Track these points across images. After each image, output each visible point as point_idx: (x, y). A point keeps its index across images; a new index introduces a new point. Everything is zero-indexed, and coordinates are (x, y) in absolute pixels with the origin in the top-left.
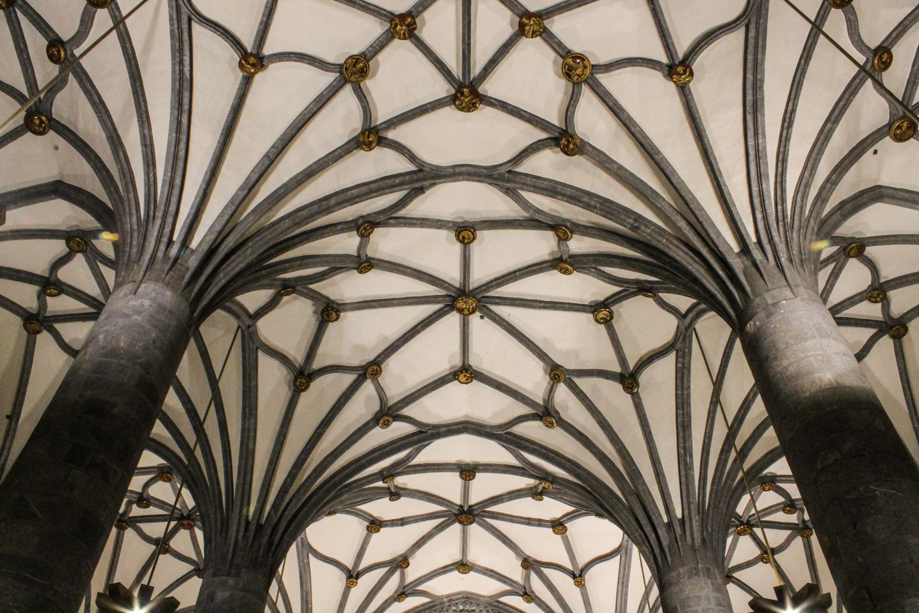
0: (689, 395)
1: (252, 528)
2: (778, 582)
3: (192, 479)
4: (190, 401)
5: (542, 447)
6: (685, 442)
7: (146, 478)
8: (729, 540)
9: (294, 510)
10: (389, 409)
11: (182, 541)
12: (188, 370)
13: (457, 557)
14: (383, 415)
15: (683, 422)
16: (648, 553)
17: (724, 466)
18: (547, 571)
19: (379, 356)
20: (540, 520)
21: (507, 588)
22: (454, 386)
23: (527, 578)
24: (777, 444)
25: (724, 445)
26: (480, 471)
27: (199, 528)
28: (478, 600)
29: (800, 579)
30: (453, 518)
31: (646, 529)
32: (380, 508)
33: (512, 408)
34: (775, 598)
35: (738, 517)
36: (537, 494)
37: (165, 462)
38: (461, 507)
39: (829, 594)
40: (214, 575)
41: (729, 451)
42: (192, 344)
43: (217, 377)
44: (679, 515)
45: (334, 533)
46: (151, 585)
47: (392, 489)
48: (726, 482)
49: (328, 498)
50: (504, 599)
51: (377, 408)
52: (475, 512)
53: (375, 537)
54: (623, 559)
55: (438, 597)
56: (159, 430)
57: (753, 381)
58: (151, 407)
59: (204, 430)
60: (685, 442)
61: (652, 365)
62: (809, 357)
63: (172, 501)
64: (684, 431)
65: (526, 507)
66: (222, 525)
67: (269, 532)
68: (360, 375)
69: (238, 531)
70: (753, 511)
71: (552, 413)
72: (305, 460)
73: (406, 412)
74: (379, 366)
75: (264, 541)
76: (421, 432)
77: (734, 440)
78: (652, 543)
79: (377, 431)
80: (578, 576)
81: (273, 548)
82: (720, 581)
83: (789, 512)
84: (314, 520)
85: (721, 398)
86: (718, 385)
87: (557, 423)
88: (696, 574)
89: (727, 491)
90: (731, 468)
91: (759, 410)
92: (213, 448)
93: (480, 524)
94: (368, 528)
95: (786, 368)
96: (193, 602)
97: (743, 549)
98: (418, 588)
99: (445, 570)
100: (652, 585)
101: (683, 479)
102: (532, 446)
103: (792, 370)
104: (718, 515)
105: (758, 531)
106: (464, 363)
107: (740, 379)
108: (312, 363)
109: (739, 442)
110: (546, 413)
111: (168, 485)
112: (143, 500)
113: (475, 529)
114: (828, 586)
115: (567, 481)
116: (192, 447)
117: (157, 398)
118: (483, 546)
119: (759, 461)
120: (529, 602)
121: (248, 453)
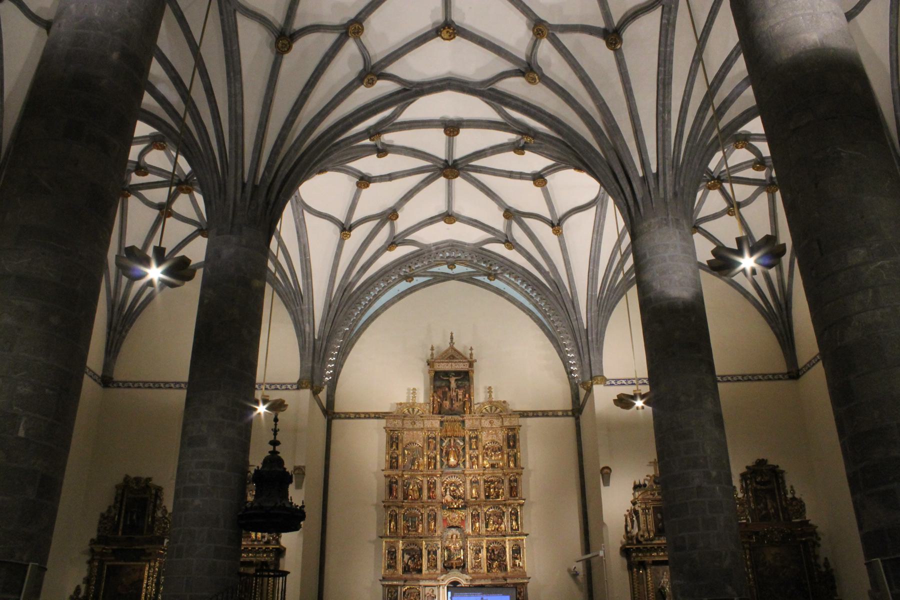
0: (671, 53)
1: (249, 189)
2: (740, 233)
3: (186, 147)
4: (173, 69)
5: (524, 102)
6: (664, 100)
7: (142, 147)
8: (699, 194)
9: (287, 171)
10: (373, 67)
11: (182, 204)
12: (168, 38)
13: (443, 209)
14: (368, 74)
15: (664, 79)
16: (622, 205)
17: (701, 124)
18: (528, 221)
19: (360, 14)
20: (521, 173)
21: (489, 236)
22: (437, 42)
23: (509, 227)
24: (754, 103)
25: (702, 103)
26: (463, 127)
27: (197, 191)
28: (463, 247)
29: (761, 230)
30: (439, 172)
31: (621, 183)
32: (369, 164)
33: (496, 65)
34: (735, 247)
35: (710, 173)
36: (518, 148)
37: (155, 131)
38: (446, 161)
39: (784, 245)
40: (218, 234)
41: (707, 109)
42: (168, 12)
43: (198, 42)
44: (654, 170)
45: (324, 190)
46: (162, 246)
47: (380, 147)
48: (701, 139)
49: (319, 157)
50: (486, 247)
51: (360, 67)
52: (460, 166)
53: (365, 191)
54: (599, 210)
55: (426, 246)
56: (148, 100)
57: (738, 40)
58: (140, 82)
59: (191, 98)
60: (664, 100)
61: (637, 21)
62: (797, 16)
63: (170, 168)
64: (664, 88)
65: (509, 161)
66: (220, 189)
67: (264, 192)
68: (342, 34)
69: (235, 193)
70: (724, 168)
71: (535, 69)
72: (293, 122)
73: (391, 69)
74: (361, 24)
75: (261, 200)
76: (405, 90)
77: (713, 99)
78: (627, 195)
79: (362, 89)
80: (556, 225)
81: (270, 207)
82: (687, 231)
83: (758, 169)
84: (306, 178)
85: (704, 56)
86: (702, 42)
87: (540, 79)
88: (667, 224)
89: (701, 147)
90: (707, 127)
91: (740, 67)
92: (202, 115)
93: (464, 178)
94: (358, 184)
95: (773, 27)
96: (202, 258)
97: (713, 201)
98: (407, 238)
99: (432, 221)
100: (625, 234)
101: (660, 135)
102: (514, 102)
103: (778, 29)
104: (692, 170)
105: (726, 186)
106: (446, 19)
107: (725, 35)
108: (292, 24)
109: (717, 101)
110: (528, 69)
111: (162, 152)
112: (142, 168)
113: (459, 183)
114: (785, 237)
115: (548, 136)
116: (182, 116)
117: (144, 70)
118: (467, 198)
119: (734, 121)
120: (510, 249)
121: (237, 117)
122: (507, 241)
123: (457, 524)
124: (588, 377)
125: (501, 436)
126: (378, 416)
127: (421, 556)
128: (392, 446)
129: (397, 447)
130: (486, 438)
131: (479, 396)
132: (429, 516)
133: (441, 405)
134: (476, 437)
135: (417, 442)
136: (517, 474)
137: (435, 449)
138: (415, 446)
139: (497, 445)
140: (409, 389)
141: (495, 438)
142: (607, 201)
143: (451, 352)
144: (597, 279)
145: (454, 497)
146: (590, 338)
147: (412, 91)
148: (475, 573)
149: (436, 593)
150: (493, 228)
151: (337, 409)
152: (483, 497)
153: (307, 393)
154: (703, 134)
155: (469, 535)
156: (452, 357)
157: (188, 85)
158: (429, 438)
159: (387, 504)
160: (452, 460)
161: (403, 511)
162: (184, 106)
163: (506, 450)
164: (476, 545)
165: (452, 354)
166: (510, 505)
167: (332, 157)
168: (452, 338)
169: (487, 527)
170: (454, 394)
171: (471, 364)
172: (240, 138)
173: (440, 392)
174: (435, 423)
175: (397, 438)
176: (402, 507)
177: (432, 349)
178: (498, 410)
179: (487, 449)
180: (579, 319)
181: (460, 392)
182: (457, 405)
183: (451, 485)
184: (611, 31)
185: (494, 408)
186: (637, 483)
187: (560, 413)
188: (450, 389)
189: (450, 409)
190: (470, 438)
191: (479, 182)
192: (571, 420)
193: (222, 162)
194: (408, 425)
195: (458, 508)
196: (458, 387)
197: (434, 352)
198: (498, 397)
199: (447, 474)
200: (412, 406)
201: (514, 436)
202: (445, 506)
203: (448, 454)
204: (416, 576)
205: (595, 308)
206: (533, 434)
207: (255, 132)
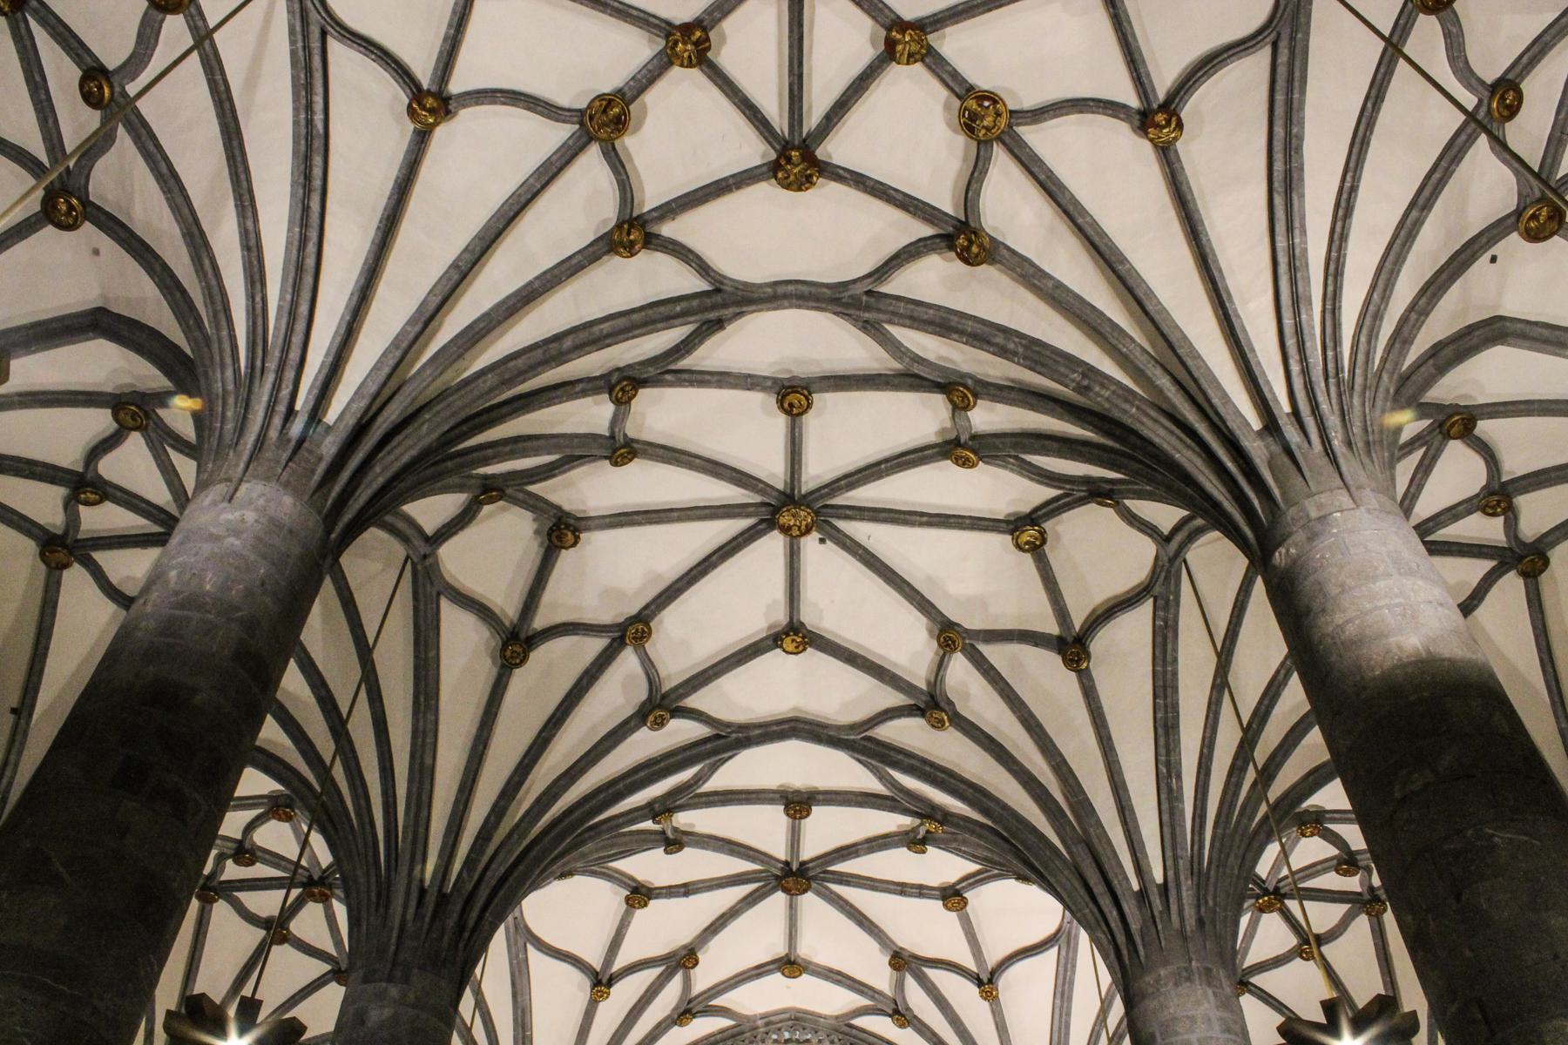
0: (1175, 674)
1: (431, 900)
2: (1328, 993)
3: (328, 817)
5: (925, 761)
7: (249, 815)
8: (1244, 921)
9: (502, 870)
10: (664, 697)
11: (310, 923)
12: (321, 630)
13: (780, 950)
15: (1166, 718)
16: (1105, 942)
17: (1236, 794)
19: (646, 607)
20: (921, 887)
21: (865, 1002)
22: (774, 658)
23: (900, 986)
24: (1326, 756)
25: (1236, 758)
28: (815, 1022)
29: (1365, 986)
30: (774, 883)
31: (1101, 902)
32: (649, 866)
33: (874, 696)
34: (1322, 1019)
35: (1259, 882)
36: (916, 842)
37: (282, 788)
38: (787, 863)
39: (1414, 1013)
40: (366, 980)
41: (1244, 770)
42: (328, 587)
43: (371, 641)
44: (1158, 876)
45: (569, 909)
46: (257, 997)
47: (670, 834)
48: (1238, 822)
50: (857, 1022)
51: (643, 695)
52: (811, 874)
53: (640, 915)
54: (1063, 953)
55: (748, 1018)
56: (271, 733)
57: (1285, 650)
58: (257, 694)
59: (347, 733)
60: (1168, 754)
64: (1167, 734)
65: (897, 864)
66: (379, 895)
67: (459, 907)
68: (614, 640)
69: (406, 906)
70: (1285, 872)
71: (942, 704)
72: (520, 784)
73: (693, 702)
74: (647, 624)
75: (451, 922)
76: (718, 737)
77: (1253, 750)
78: (1113, 925)
79: (643, 734)
80: (986, 982)
81: (466, 935)
82: (1228, 990)
83: (1346, 873)
84: (535, 886)
85: (1230, 679)
87: (950, 720)
88: (1188, 979)
89: (1241, 837)
90: (1248, 798)
91: (1294, 699)
92: (363, 764)
93: (818, 894)
94: (627, 899)
95: (1341, 627)
97: (1268, 935)
98: (713, 1003)
99: (759, 971)
101: (1166, 817)
103: (1351, 630)
104: (1225, 879)
105: (1293, 905)
106: (791, 618)
107: (1263, 646)
109: (1261, 754)
110: (932, 704)
111: (286, 826)
112: (244, 852)
113: (810, 902)
114: (1414, 998)
116: (328, 762)
117: (268, 679)
118: (824, 932)
119: (1294, 787)
120: (902, 1026)
121: (423, 773)
122: (896, 1012)
142: (1077, 936)
147: (721, 302)
150: (870, 988)
154: (1241, 814)
157: (344, 711)
162: (333, 747)
167: (584, 849)
172: (427, 782)
184: (1070, 639)
191: (846, 902)
193: (388, 849)
207: (453, 799)
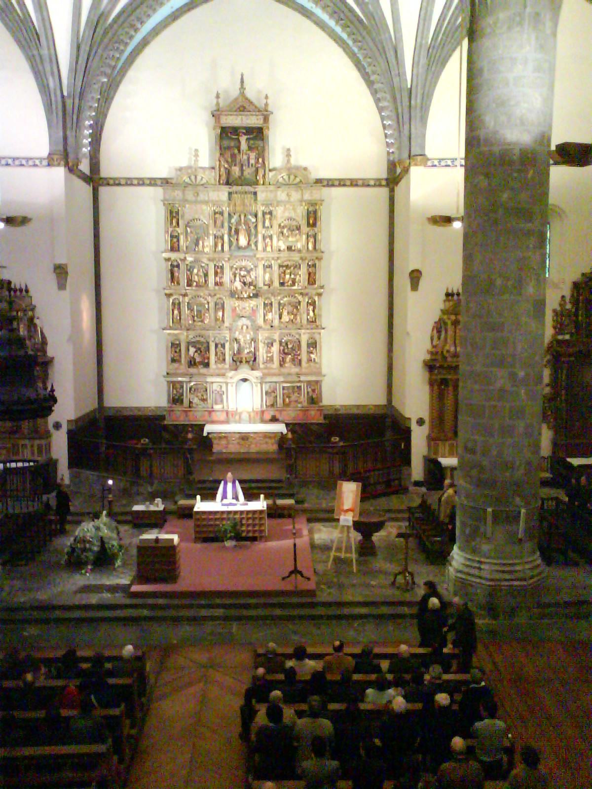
88: (520, 24)
123: (247, 314)
124: (406, 155)
125: (299, 213)
126: (153, 182)
127: (208, 349)
128: (171, 223)
129: (178, 223)
130: (281, 214)
131: (275, 159)
132: (216, 304)
133: (228, 173)
134: (270, 213)
135: (202, 218)
136: (317, 258)
137: (222, 226)
138: (199, 223)
139: (294, 223)
140: (190, 149)
141: (293, 215)
143: (241, 102)
144: (430, 19)
145: (244, 283)
146: (413, 102)
148: (266, 368)
149: (224, 389)
151: (104, 173)
152: (276, 284)
153: (59, 172)
155: (260, 327)
156: (242, 109)
158: (215, 213)
159: (167, 292)
160: (243, 241)
161: (187, 299)
163: (305, 229)
164: (267, 338)
165: (243, 105)
166: (307, 294)
168: (242, 82)
169: (280, 318)
170: (245, 157)
171: (266, 119)
173: (228, 154)
174: (222, 194)
175: (177, 213)
176: (185, 295)
177: (218, 97)
178: (298, 178)
179: (283, 227)
180: (401, 75)
181: (253, 155)
182: (248, 172)
183: (241, 269)
185: (292, 177)
186: (450, 291)
187: (372, 183)
188: (239, 151)
189: (240, 177)
190: (264, 214)
192: (384, 192)
194: (190, 195)
195: (249, 297)
196: (250, 148)
197: (220, 101)
198: (297, 160)
199: (236, 257)
200: (192, 171)
201: (315, 212)
202: (233, 294)
203: (237, 232)
204: (203, 370)
205: (423, 61)
206: (338, 208)
